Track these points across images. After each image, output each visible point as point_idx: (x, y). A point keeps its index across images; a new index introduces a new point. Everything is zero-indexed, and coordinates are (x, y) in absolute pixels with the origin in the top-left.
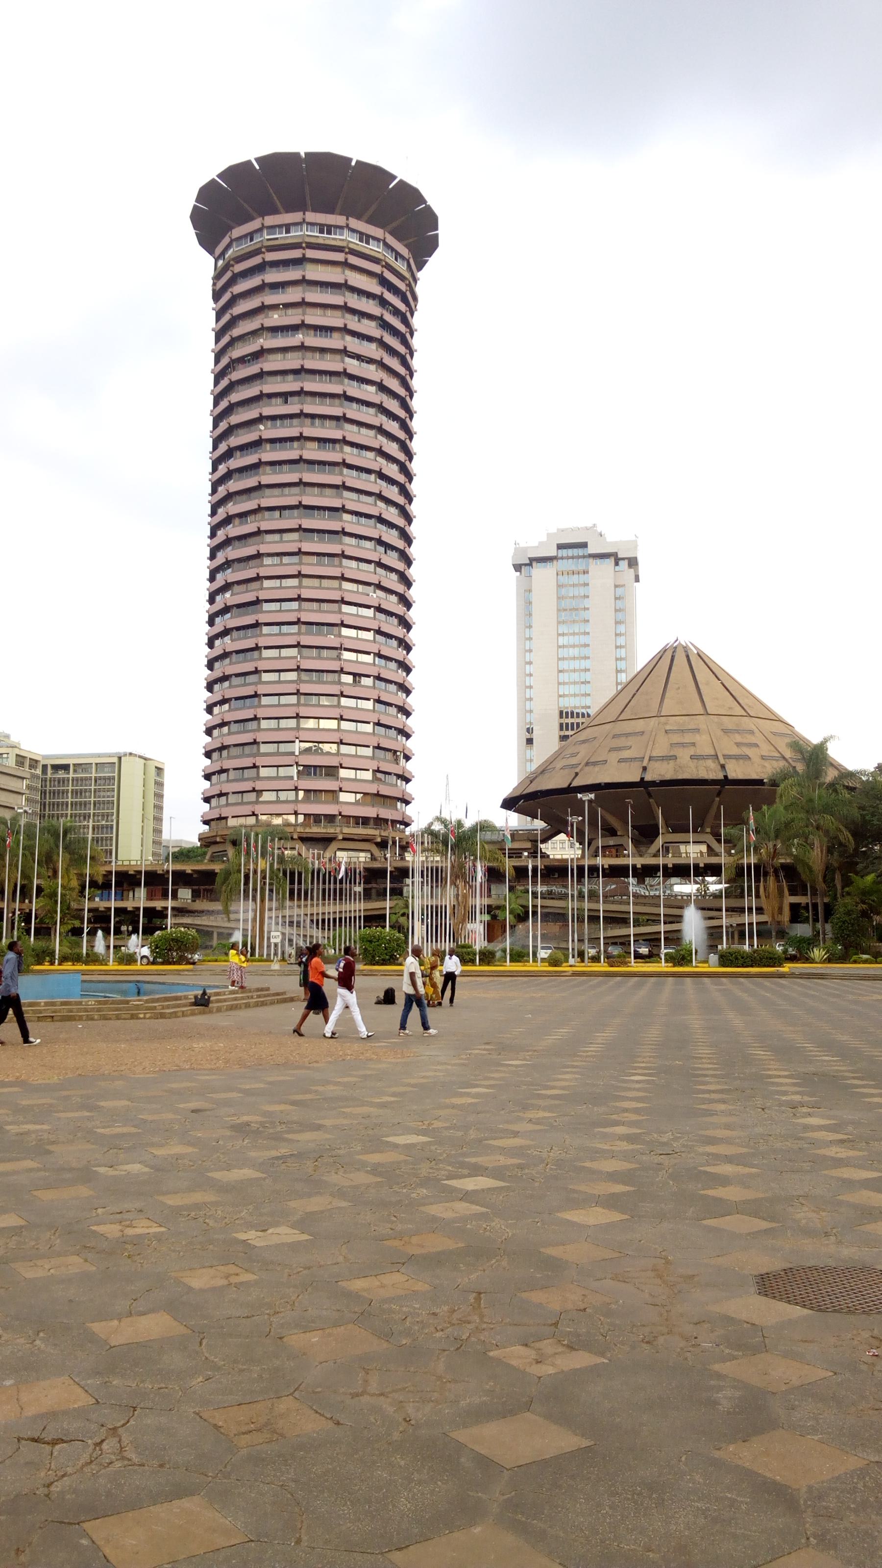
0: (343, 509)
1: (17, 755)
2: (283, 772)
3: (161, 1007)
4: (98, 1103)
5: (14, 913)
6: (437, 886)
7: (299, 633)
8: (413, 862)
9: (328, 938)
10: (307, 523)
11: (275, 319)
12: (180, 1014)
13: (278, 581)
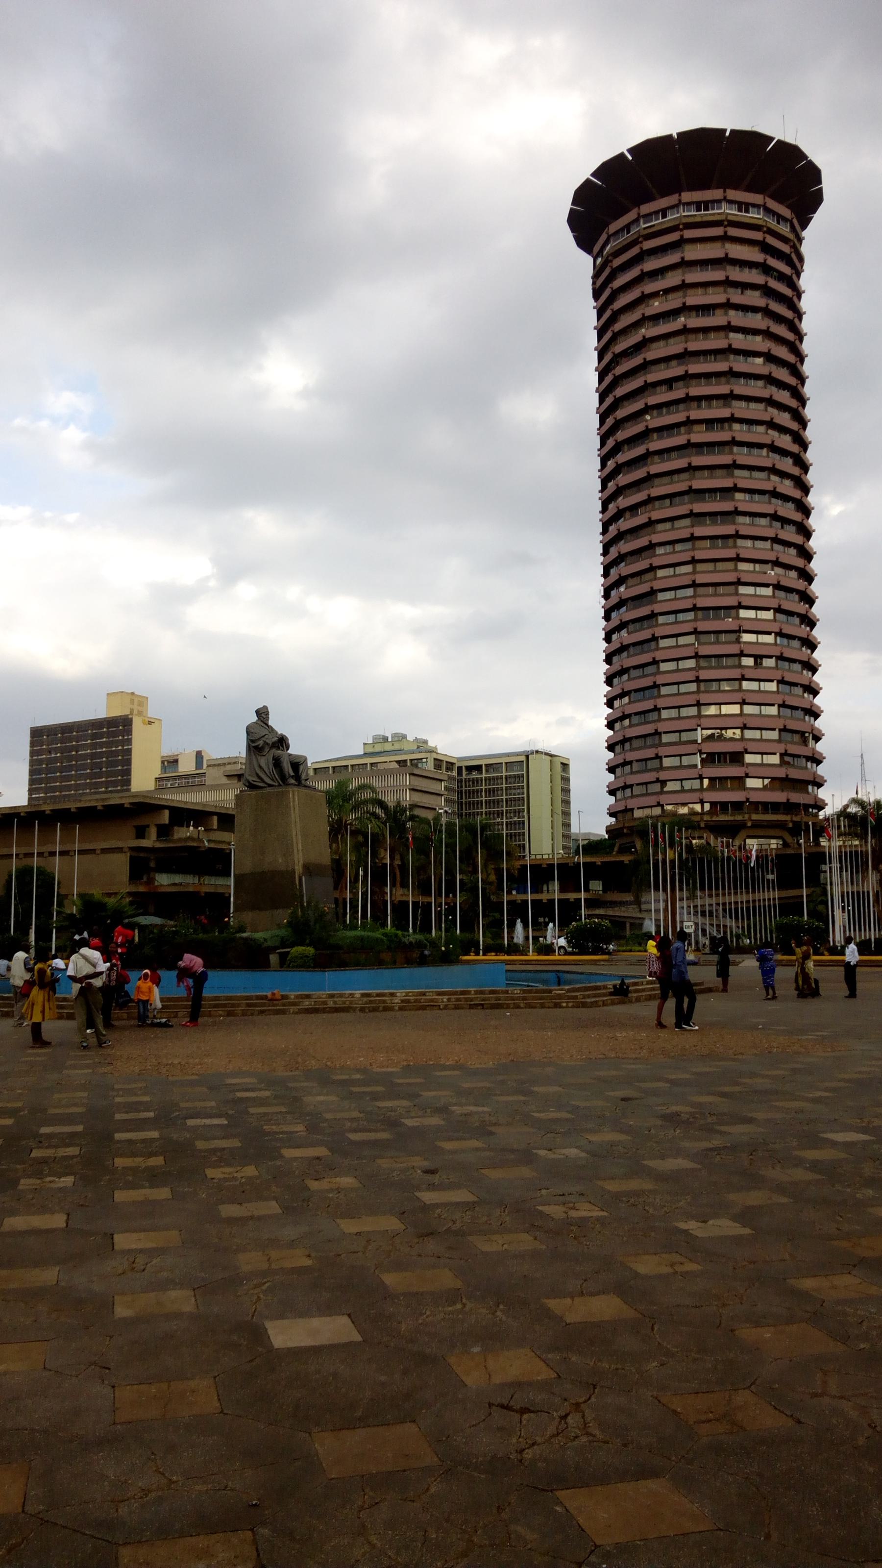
0: (736, 489)
1: (435, 759)
2: (686, 761)
3: (581, 997)
4: (532, 1088)
5: (441, 906)
6: (857, 872)
7: (696, 620)
8: (830, 847)
9: (743, 927)
10: (698, 508)
11: (656, 306)
12: (601, 1003)
13: (672, 569)
